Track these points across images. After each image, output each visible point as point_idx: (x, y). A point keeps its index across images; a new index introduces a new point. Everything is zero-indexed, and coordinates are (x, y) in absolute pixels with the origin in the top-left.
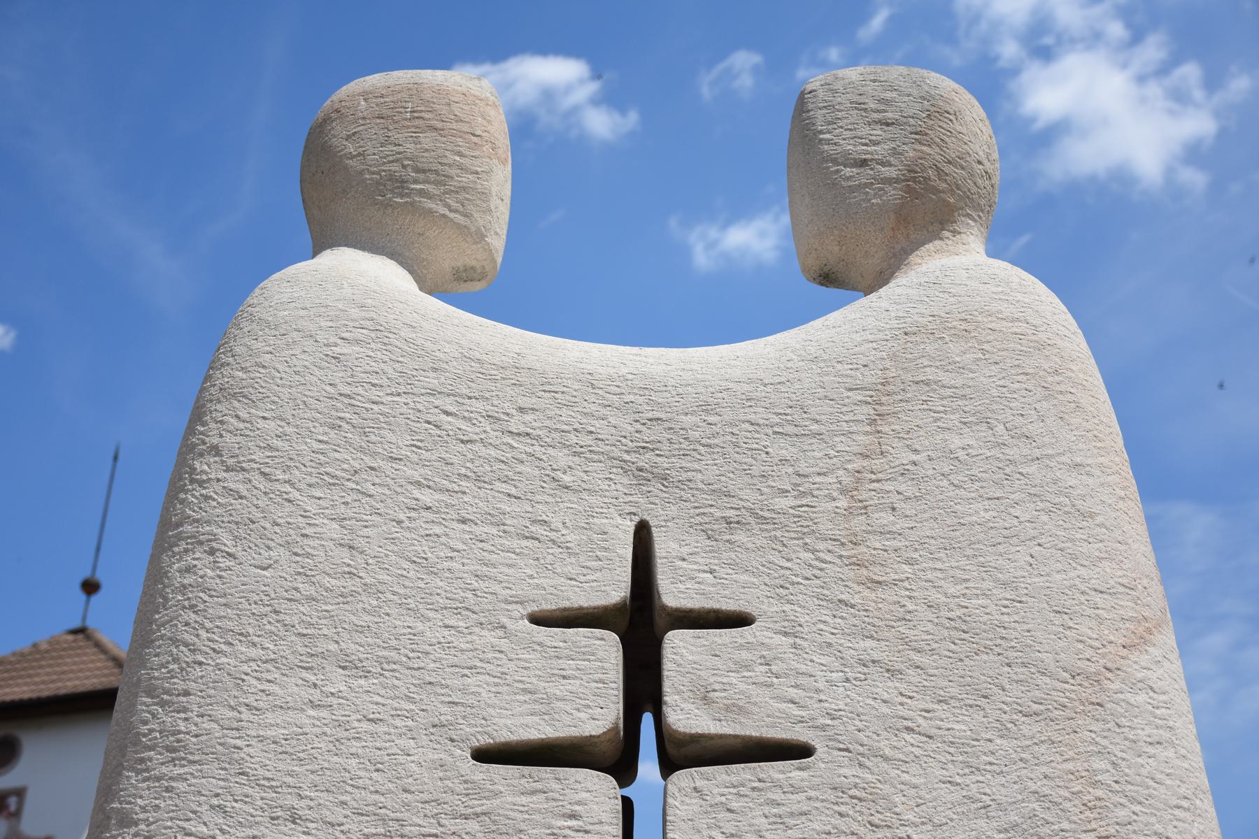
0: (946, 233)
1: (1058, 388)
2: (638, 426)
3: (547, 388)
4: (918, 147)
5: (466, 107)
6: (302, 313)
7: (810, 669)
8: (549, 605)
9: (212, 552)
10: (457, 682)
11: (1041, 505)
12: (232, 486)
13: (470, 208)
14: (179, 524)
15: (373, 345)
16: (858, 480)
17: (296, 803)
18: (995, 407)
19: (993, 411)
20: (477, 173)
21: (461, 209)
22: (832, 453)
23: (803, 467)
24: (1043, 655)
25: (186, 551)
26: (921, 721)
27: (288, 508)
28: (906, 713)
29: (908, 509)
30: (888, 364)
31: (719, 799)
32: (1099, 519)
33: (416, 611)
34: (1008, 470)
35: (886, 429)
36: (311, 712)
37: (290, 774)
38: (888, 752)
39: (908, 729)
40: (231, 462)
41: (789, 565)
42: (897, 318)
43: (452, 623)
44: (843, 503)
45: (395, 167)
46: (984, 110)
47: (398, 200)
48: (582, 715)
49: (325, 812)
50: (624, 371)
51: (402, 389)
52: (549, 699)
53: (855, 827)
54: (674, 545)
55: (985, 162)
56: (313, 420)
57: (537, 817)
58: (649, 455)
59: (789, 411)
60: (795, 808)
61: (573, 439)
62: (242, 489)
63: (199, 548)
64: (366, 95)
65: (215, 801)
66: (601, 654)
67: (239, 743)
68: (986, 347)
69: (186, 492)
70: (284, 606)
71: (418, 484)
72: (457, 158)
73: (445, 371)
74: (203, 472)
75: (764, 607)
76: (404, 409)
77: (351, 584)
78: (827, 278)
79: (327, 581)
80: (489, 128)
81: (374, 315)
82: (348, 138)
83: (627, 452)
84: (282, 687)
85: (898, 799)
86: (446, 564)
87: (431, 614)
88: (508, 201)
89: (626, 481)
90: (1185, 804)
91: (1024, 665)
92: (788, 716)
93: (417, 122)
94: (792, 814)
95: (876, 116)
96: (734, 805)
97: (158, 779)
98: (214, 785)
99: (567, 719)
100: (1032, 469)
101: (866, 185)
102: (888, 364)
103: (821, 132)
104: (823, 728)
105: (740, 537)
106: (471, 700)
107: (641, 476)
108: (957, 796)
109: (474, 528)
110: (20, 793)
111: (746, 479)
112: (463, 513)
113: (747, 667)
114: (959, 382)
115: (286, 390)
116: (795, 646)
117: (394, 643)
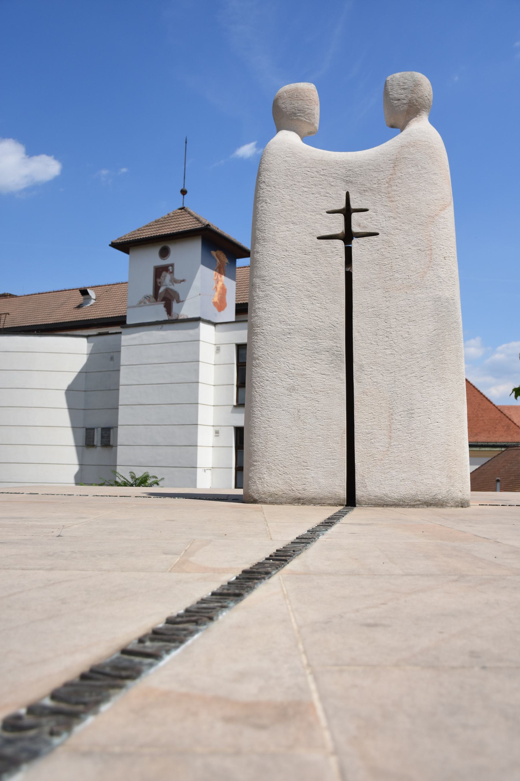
0: (418, 116)
1: (433, 156)
2: (346, 171)
3: (328, 164)
5: (308, 93)
6: (278, 151)
8: (330, 210)
9: (266, 203)
11: (426, 183)
12: (268, 189)
13: (310, 118)
15: (293, 158)
16: (390, 180)
17: (286, 248)
18: (418, 162)
19: (418, 163)
21: (308, 119)
22: (385, 175)
23: (379, 178)
24: (424, 213)
25: (261, 203)
26: (399, 227)
27: (280, 193)
29: (400, 185)
31: (361, 243)
32: (438, 185)
34: (420, 176)
35: (396, 169)
36: (288, 232)
37: (285, 243)
38: (393, 233)
39: (397, 229)
40: (267, 184)
41: (376, 199)
42: (400, 143)
43: (312, 214)
45: (293, 110)
47: (295, 118)
48: (337, 230)
49: (292, 249)
50: (344, 159)
51: (299, 167)
52: (331, 227)
53: (386, 247)
54: (353, 196)
55: (428, 96)
56: (282, 175)
57: (329, 248)
58: (349, 178)
59: (377, 166)
60: (375, 244)
61: (333, 175)
62: (270, 190)
63: (263, 202)
64: (286, 92)
65: (273, 248)
66: (340, 218)
67: (275, 238)
68: (418, 148)
69: (260, 191)
70: (281, 213)
71: (304, 187)
72: (307, 106)
73: (307, 162)
75: (371, 207)
76: (300, 171)
77: (293, 208)
78: (392, 127)
79: (288, 207)
80: (314, 97)
81: (292, 150)
83: (344, 177)
84: (282, 228)
85: (394, 242)
86: (310, 203)
87: (308, 213)
88: (319, 114)
89: (344, 183)
90: (447, 239)
91: (420, 215)
92: (374, 228)
93: (297, 98)
94: (374, 245)
95: (402, 87)
96: (364, 244)
97: (262, 245)
98: (272, 246)
99: (334, 231)
100: (425, 175)
101: (400, 105)
102: (397, 154)
103: (390, 92)
104: (381, 230)
105: (366, 193)
106: (316, 228)
107: (347, 182)
108: (405, 240)
110: (172, 265)
111: (368, 181)
112: (313, 192)
113: (367, 219)
114: (412, 157)
115: (276, 169)
116: (376, 215)
117: (301, 218)
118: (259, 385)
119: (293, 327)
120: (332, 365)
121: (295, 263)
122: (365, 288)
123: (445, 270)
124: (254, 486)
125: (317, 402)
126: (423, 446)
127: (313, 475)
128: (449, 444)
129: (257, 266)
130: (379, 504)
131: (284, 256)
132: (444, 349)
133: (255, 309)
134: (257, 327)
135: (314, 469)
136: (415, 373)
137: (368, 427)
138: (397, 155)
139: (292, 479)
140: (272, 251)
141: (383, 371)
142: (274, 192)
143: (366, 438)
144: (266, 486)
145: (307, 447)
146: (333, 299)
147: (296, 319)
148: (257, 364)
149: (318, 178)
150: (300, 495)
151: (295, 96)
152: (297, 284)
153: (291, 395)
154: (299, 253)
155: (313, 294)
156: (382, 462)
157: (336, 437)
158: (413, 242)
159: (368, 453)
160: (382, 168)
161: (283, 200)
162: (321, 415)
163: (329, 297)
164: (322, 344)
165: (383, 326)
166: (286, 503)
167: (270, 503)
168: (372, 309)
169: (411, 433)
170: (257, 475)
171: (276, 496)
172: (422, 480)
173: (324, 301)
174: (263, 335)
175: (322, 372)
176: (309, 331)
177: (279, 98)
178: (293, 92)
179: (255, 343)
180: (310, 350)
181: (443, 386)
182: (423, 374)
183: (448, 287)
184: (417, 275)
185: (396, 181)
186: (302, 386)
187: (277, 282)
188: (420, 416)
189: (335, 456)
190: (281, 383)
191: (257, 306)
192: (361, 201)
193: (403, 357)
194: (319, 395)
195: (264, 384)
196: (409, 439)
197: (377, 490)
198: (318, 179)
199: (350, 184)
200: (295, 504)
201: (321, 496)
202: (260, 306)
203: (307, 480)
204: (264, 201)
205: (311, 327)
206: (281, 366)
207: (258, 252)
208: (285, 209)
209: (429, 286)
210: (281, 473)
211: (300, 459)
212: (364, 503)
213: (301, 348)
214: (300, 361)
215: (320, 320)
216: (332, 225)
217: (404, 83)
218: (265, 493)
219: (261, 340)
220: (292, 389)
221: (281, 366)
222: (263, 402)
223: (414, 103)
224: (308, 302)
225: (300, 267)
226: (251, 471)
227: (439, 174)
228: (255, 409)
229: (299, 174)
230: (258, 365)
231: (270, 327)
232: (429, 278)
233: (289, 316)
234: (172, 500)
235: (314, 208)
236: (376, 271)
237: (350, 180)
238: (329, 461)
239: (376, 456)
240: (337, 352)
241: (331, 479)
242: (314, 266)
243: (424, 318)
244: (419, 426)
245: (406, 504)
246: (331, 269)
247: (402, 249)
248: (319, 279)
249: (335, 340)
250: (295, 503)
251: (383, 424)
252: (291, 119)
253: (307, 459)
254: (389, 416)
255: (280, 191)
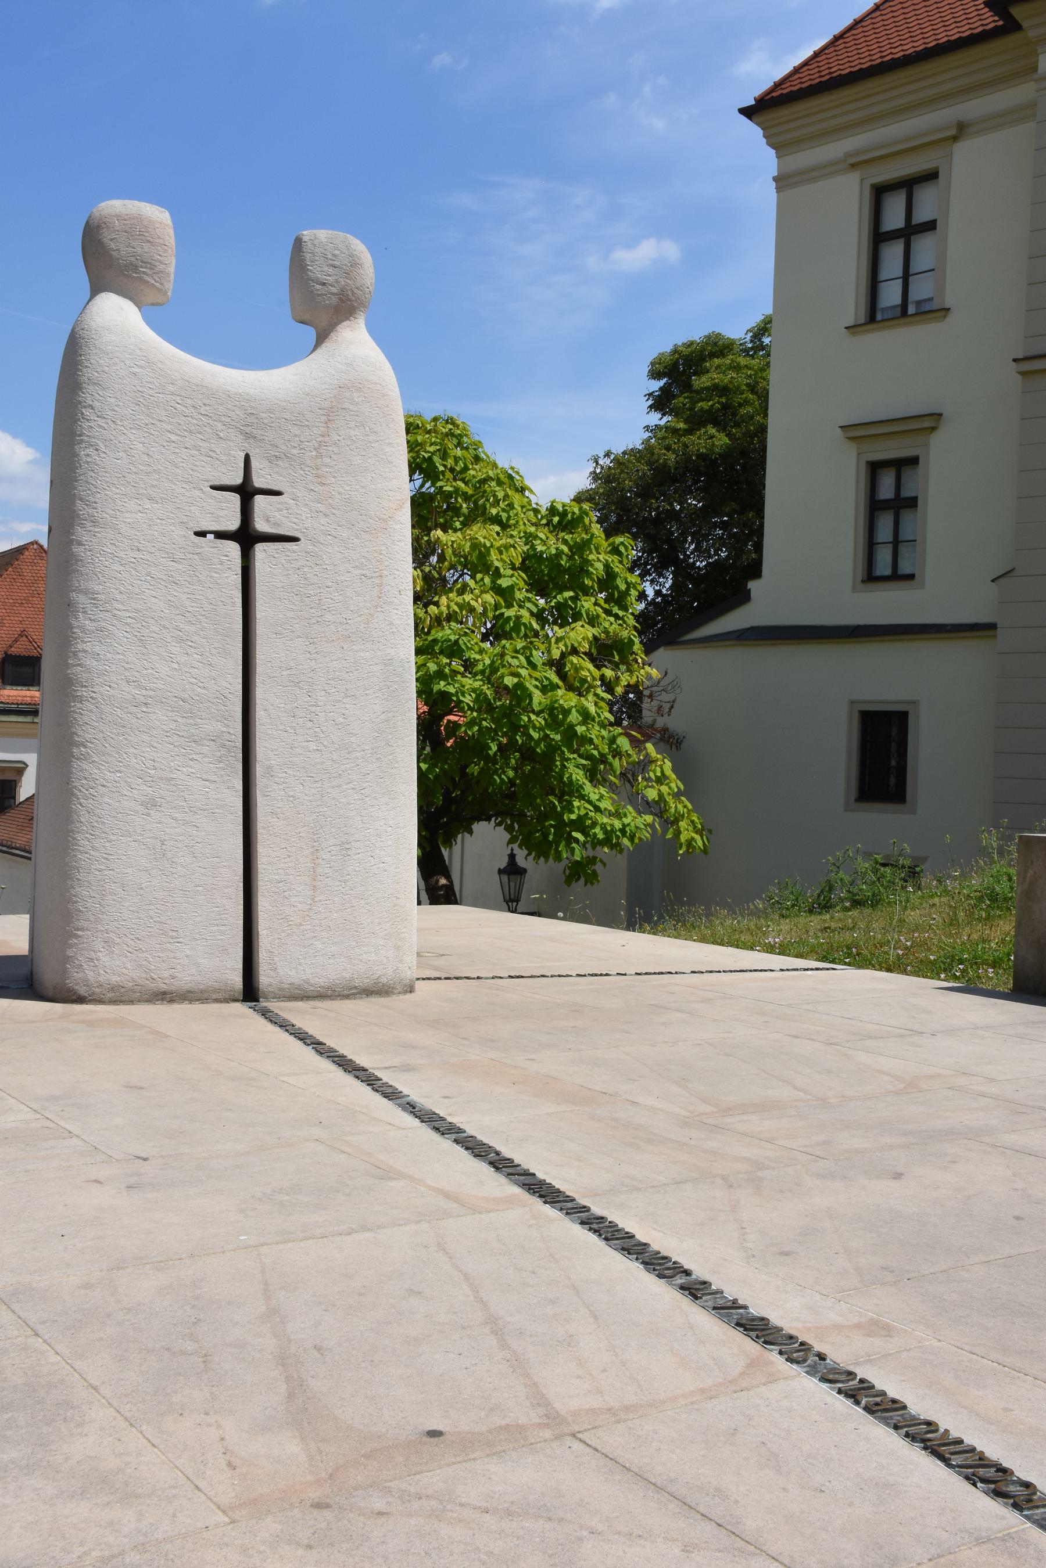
4: (345, 280)
6: (117, 349)
7: (300, 512)
8: (217, 483)
9: (97, 450)
10: (187, 508)
11: (377, 459)
13: (163, 281)
14: (80, 435)
16: (320, 445)
18: (366, 420)
20: (166, 264)
23: (302, 439)
25: (86, 447)
27: (124, 437)
28: (329, 529)
30: (333, 400)
33: (172, 481)
35: (330, 426)
36: (140, 514)
37: (136, 535)
38: (323, 542)
39: (329, 535)
40: (99, 414)
42: (337, 380)
44: (314, 453)
45: (133, 259)
46: (390, 363)
48: (229, 523)
54: (258, 464)
61: (223, 419)
62: (105, 426)
63: (91, 447)
65: (112, 542)
66: (234, 502)
67: (117, 523)
68: (366, 395)
71: (170, 432)
74: (87, 415)
77: (149, 469)
81: (145, 354)
82: (111, 240)
85: (324, 556)
86: (181, 464)
87: (177, 483)
91: (365, 515)
92: (293, 528)
93: (141, 237)
94: (293, 560)
95: (330, 262)
96: (276, 556)
97: (90, 531)
102: (333, 400)
103: (308, 265)
104: (304, 533)
105: (280, 463)
107: (248, 436)
109: (190, 451)
113: (281, 511)
114: (355, 409)
115: (117, 386)
116: (296, 504)
117: (165, 492)
118: (87, 792)
119: (152, 693)
120: (221, 765)
121: (154, 576)
122: (276, 633)
123: (400, 613)
124: (77, 972)
125: (195, 829)
126: (362, 902)
127: (188, 952)
128: (398, 895)
129: (78, 571)
130: (296, 996)
131: (134, 560)
132: (395, 745)
133: (77, 652)
134: (82, 686)
135: (189, 943)
136: (354, 783)
137: (280, 871)
138: (332, 402)
139: (151, 960)
140: (109, 546)
141: (304, 778)
142: (114, 433)
143: (277, 890)
144: (102, 972)
145: (177, 905)
146: (224, 649)
147: (157, 678)
148: (82, 754)
149: (196, 419)
150: (165, 987)
151: (136, 228)
152: (159, 615)
153: (148, 815)
154: (163, 558)
155: (188, 636)
156: (301, 928)
157: (227, 887)
158: (353, 560)
159: (279, 914)
160: (308, 421)
161: (132, 451)
162: (201, 850)
163: (216, 645)
164: (203, 728)
165: (305, 702)
166: (139, 1001)
167: (110, 1002)
168: (288, 672)
169: (345, 881)
170: (86, 953)
171: (123, 990)
172: (360, 955)
173: (207, 652)
174: (94, 701)
175: (205, 776)
176: (182, 703)
177: (104, 226)
178: (132, 221)
179: (76, 716)
180: (183, 736)
181: (392, 805)
182: (364, 785)
183: (403, 642)
184: (359, 619)
185: (330, 448)
186: (169, 799)
187: (119, 606)
188: (359, 853)
189: (226, 920)
190: (130, 793)
191: (80, 647)
192: (270, 475)
193: (335, 756)
194: (198, 817)
195: (96, 792)
196: (343, 890)
197: (293, 973)
198: (195, 422)
199: (252, 441)
200: (157, 1003)
201: (202, 987)
202: (87, 647)
203: (178, 961)
204: (92, 445)
205: (184, 695)
206: (129, 762)
207: (80, 544)
208: (135, 470)
209: (377, 639)
210: (130, 950)
211: (165, 925)
212: (273, 995)
213: (167, 732)
214: (165, 755)
215: (201, 685)
216: (221, 513)
217: (334, 255)
218: (101, 985)
219: (91, 711)
220: (151, 804)
221: (129, 762)
222: (95, 824)
223: (348, 295)
224: (178, 649)
225: (164, 583)
226: (71, 946)
227: (395, 446)
228: (78, 836)
229: (161, 404)
230: (86, 757)
231: (109, 689)
232: (377, 626)
233: (145, 672)
234: (338, 1073)
235: (188, 475)
236: (296, 606)
237: (252, 432)
238: (216, 928)
239: (292, 919)
240: (230, 743)
241: (218, 959)
242: (188, 586)
243: (368, 692)
244: (357, 869)
245: (337, 994)
246: (220, 593)
247: (337, 571)
248: (198, 609)
249: (226, 722)
250: (157, 1000)
251: (303, 866)
252: (127, 275)
253: (177, 926)
254: (312, 854)
255: (125, 431)
